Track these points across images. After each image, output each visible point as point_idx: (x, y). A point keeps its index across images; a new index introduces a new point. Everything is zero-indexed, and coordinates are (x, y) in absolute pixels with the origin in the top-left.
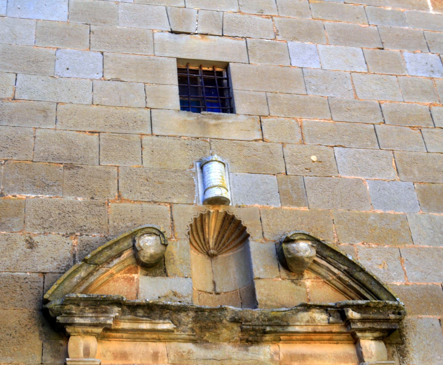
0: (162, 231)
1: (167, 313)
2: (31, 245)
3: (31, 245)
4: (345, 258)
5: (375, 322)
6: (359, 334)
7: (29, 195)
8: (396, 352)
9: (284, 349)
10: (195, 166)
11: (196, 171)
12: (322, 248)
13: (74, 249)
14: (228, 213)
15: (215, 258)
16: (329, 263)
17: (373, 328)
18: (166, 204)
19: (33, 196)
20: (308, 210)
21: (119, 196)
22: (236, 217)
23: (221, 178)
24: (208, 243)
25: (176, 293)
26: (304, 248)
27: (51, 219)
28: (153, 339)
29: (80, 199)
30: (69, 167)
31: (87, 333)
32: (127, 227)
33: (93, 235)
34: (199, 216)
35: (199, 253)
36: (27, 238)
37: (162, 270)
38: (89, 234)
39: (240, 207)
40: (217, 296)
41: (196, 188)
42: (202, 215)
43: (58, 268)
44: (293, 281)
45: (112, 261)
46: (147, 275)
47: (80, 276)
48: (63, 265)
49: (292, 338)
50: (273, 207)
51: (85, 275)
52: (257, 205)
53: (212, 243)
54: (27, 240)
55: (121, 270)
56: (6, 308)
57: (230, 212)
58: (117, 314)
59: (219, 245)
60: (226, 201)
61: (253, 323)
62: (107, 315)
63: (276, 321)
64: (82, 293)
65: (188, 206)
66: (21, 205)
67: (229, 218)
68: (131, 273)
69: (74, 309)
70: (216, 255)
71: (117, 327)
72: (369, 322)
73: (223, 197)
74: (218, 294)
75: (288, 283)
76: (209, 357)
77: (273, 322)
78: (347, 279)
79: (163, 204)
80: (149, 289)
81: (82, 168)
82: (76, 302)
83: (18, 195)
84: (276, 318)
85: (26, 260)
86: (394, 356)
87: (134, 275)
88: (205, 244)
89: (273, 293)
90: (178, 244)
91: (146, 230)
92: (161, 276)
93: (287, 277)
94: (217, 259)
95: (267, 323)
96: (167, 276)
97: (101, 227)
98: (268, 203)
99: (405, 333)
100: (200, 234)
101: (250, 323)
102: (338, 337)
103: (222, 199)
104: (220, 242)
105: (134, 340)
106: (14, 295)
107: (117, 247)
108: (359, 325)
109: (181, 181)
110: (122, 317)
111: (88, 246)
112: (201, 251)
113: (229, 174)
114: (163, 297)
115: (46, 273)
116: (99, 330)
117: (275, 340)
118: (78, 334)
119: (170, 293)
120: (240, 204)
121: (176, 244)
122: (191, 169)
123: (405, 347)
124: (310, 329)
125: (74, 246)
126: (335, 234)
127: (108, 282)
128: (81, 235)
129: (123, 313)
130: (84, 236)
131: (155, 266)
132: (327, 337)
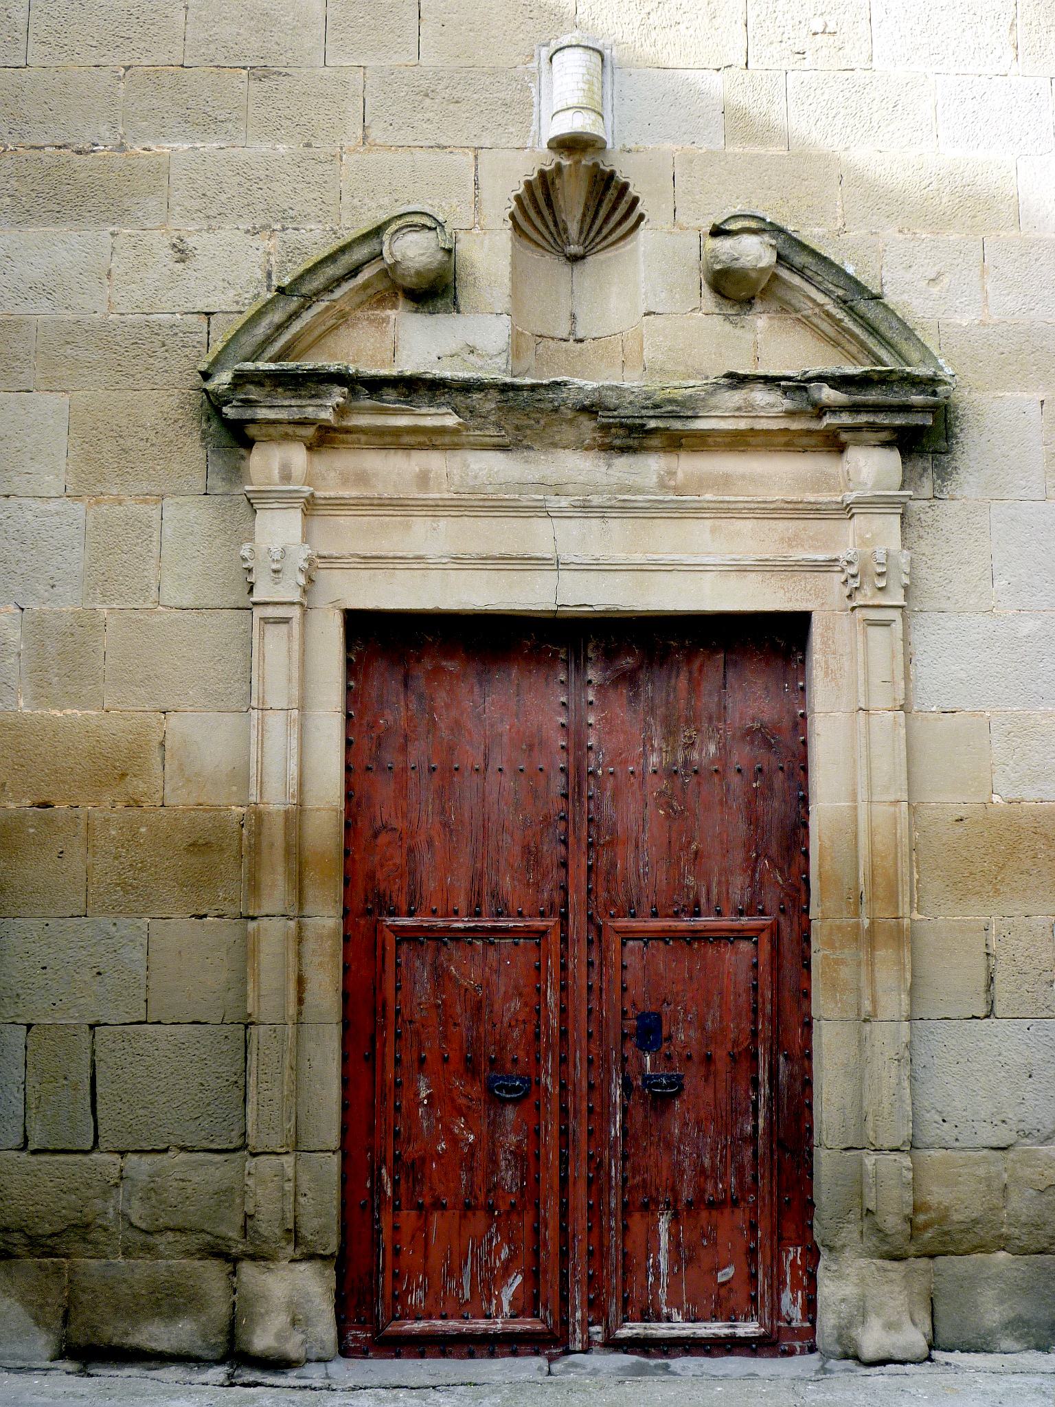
0: (440, 219)
1: (443, 394)
2: (182, 253)
3: (182, 253)
4: (840, 271)
5: (881, 412)
6: (844, 437)
7: (175, 145)
8: (930, 471)
9: (688, 465)
10: (536, 57)
12: (793, 252)
13: (268, 261)
14: (602, 167)
15: (580, 263)
16: (808, 280)
17: (873, 423)
19: (186, 146)
20: (786, 153)
21: (365, 137)
23: (586, 87)
24: (566, 230)
26: (753, 252)
27: (223, 197)
28: (419, 444)
29: (282, 148)
30: (260, 73)
31: (286, 438)
32: (380, 207)
33: (308, 227)
34: (536, 175)
36: (175, 241)
38: (300, 226)
40: (580, 345)
41: (536, 109)
42: (542, 174)
43: (237, 303)
44: (727, 317)
45: (339, 285)
46: (416, 312)
47: (271, 322)
48: (247, 296)
49: (702, 442)
50: (705, 146)
51: (282, 320)
52: (668, 146)
53: (573, 228)
54: (174, 246)
55: (362, 303)
56: (137, 387)
58: (341, 400)
59: (588, 234)
61: (622, 412)
62: (319, 402)
63: (670, 408)
64: (271, 360)
66: (160, 171)
68: (384, 308)
69: (254, 393)
70: (583, 257)
71: (344, 423)
72: (868, 412)
74: (581, 341)
76: (530, 478)
77: (663, 410)
78: (840, 315)
80: (416, 344)
81: (287, 74)
82: (258, 379)
83: (153, 147)
84: (671, 401)
85: (172, 288)
86: (924, 479)
87: (389, 312)
90: (486, 242)
91: (408, 219)
92: (445, 312)
93: (717, 311)
95: (651, 413)
96: (458, 312)
97: (325, 208)
99: (957, 430)
100: (546, 212)
101: (615, 413)
102: (805, 441)
104: (591, 227)
105: (384, 447)
106: (151, 361)
107: (346, 257)
108: (846, 419)
109: (502, 95)
110: (354, 404)
111: (297, 252)
115: (213, 313)
116: (310, 432)
117: (669, 446)
118: (271, 439)
120: (633, 146)
121: (482, 243)
123: (953, 459)
124: (742, 425)
125: (269, 253)
126: (840, 211)
127: (337, 328)
128: (284, 229)
129: (354, 393)
130: (290, 231)
131: (434, 291)
132: (783, 439)
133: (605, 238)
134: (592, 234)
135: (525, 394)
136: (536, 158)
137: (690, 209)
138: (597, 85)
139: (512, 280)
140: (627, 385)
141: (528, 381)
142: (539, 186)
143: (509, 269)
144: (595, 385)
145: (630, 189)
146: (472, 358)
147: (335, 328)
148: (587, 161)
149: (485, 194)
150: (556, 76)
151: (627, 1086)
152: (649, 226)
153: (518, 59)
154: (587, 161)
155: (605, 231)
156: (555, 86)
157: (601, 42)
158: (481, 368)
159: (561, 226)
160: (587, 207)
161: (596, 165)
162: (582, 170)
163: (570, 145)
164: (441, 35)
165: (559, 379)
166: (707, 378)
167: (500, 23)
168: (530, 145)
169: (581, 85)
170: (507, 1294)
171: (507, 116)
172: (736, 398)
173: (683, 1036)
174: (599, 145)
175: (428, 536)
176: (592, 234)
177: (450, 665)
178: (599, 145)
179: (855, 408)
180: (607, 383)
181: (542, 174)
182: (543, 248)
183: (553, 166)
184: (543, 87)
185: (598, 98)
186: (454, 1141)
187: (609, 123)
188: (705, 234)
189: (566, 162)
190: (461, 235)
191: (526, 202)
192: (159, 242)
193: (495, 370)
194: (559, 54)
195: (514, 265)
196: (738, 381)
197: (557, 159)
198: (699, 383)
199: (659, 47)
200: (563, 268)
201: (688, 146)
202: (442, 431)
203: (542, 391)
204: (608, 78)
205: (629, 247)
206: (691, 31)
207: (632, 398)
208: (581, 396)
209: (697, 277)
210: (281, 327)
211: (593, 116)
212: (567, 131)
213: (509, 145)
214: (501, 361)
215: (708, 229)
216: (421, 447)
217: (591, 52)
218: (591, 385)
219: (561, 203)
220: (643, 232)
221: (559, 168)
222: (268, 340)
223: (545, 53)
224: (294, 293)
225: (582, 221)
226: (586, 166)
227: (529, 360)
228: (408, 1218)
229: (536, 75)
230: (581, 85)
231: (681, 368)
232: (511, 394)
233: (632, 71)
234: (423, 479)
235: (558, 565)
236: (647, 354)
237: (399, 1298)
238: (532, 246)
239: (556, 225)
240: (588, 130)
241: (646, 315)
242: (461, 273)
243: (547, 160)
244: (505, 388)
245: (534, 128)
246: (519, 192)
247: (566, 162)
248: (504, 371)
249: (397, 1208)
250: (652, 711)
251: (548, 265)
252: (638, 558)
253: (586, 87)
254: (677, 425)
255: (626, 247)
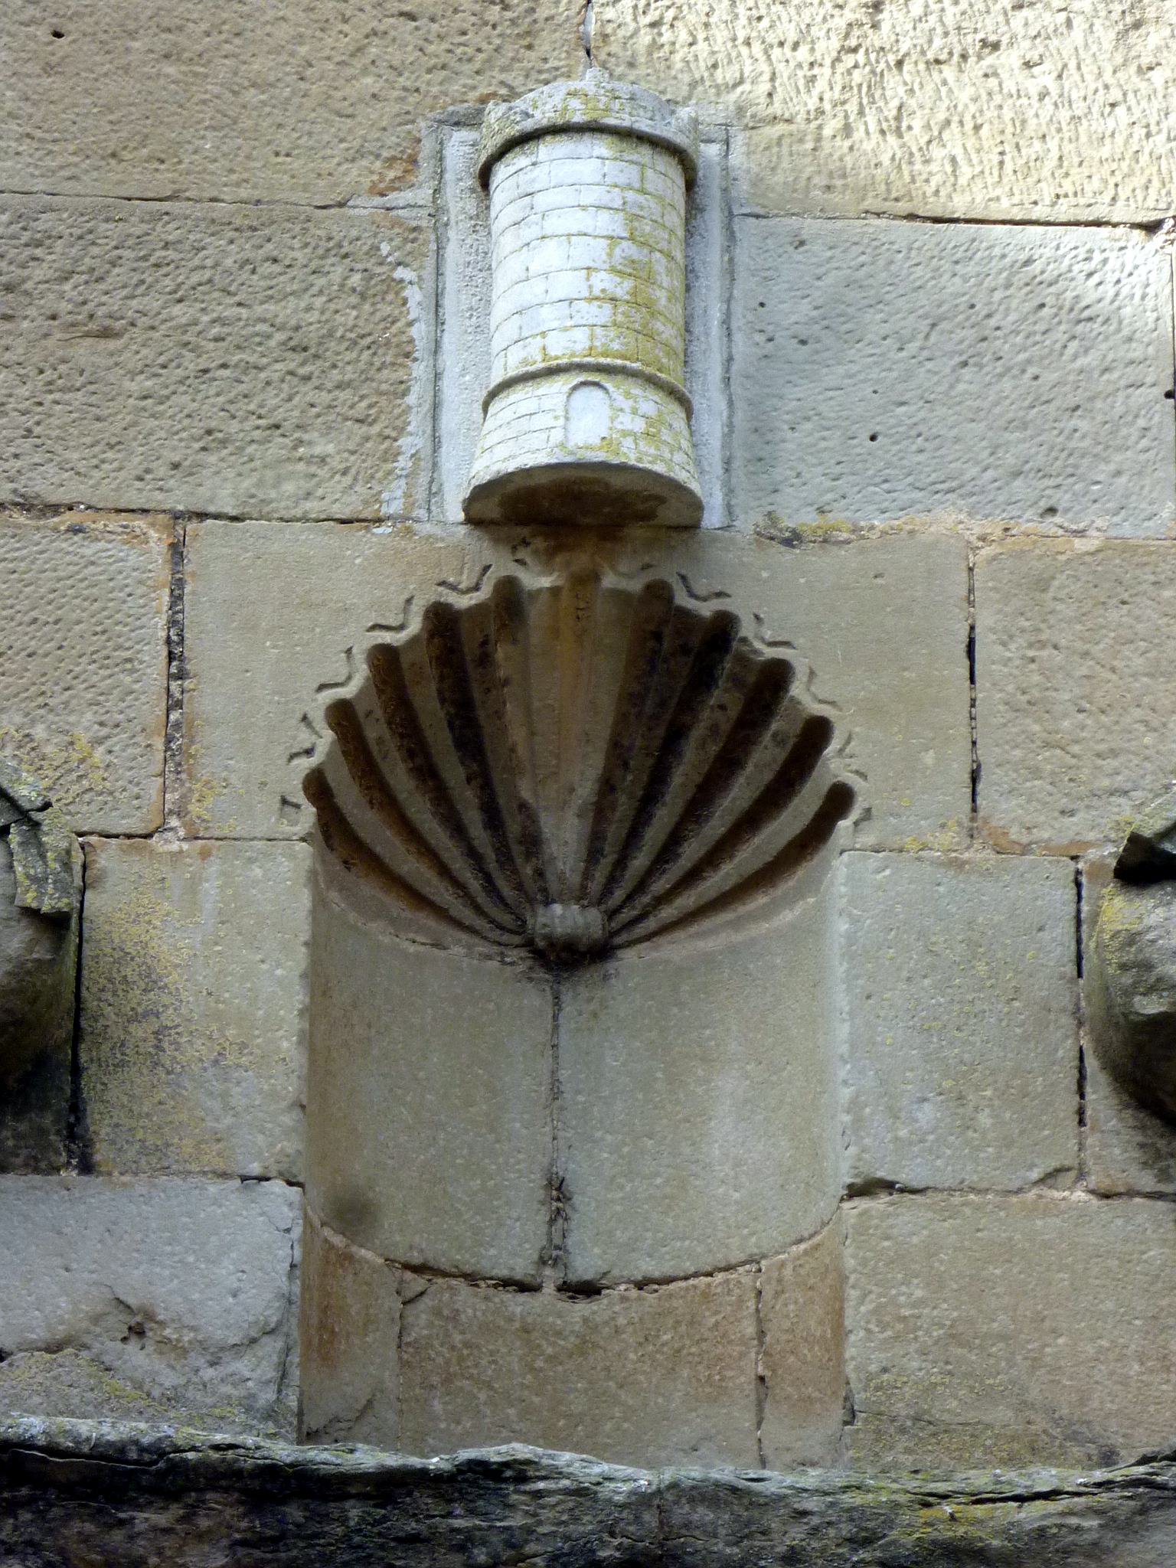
10: (426, 168)
11: (437, 212)
14: (682, 599)
18: (139, 523)
22: (747, 629)
23: (622, 288)
24: (533, 842)
25: (150, 1316)
35: (451, 934)
37: (48, 1120)
39: (793, 540)
40: (582, 1308)
41: (420, 370)
42: (441, 619)
50: (1099, 528)
52: (947, 519)
53: (564, 837)
57: (701, 587)
59: (621, 863)
60: (436, 614)
65: (335, 538)
67: (695, 641)
73: (623, 468)
74: (588, 1290)
79: (114, 523)
88: (505, 858)
89: (1002, 1322)
90: (210, 888)
92: (34, 1166)
93: (1147, 1181)
94: (606, 978)
96: (87, 1167)
98: (1062, 499)
100: (453, 771)
103: (617, 481)
104: (633, 836)
109: (286, 311)
112: (467, 915)
113: (731, 235)
114: (32, 1348)
119: (96, 1319)
120: (806, 519)
121: (193, 887)
122: (395, 198)
133: (693, 876)
134: (640, 862)
135: (354, 1512)
136: (447, 561)
137: (1036, 772)
138: (668, 280)
139: (310, 1042)
140: (777, 1480)
141: (368, 1458)
142: (431, 671)
143: (299, 997)
144: (645, 1480)
145: (797, 689)
146: (137, 1358)
148: (621, 577)
149: (208, 698)
150: (506, 243)
152: (868, 838)
153: (356, 174)
154: (621, 577)
155: (691, 851)
156: (502, 279)
157: (685, 113)
158: (173, 1399)
159: (513, 827)
160: (618, 754)
161: (658, 592)
162: (602, 611)
163: (543, 509)
164: (49, 69)
165: (494, 1453)
166: (1108, 1458)
167: (283, 32)
168: (395, 508)
169: (603, 281)
171: (307, 393)
174: (669, 514)
176: (640, 862)
178: (669, 514)
180: (692, 1472)
181: (441, 619)
182: (441, 913)
183: (484, 594)
184: (451, 281)
185: (668, 332)
187: (712, 425)
188: (1097, 868)
189: (537, 580)
190: (108, 858)
191: (375, 731)
193: (227, 1410)
194: (518, 160)
195: (319, 981)
197: (504, 566)
198: (1079, 1478)
199: (916, 137)
200: (518, 998)
201: (1029, 523)
203: (426, 1501)
204: (713, 256)
205: (787, 916)
206: (1044, 76)
207: (796, 1535)
208: (587, 1525)
209: (1064, 1042)
211: (650, 402)
212: (542, 459)
213: (312, 506)
214: (254, 1371)
215: (1109, 853)
217: (645, 154)
218: (628, 1478)
219: (517, 734)
220: (847, 866)
221: (509, 601)
223: (461, 150)
225: (600, 810)
226: (618, 595)
227: (370, 1366)
229: (424, 238)
230: (603, 281)
231: (1002, 1414)
232: (295, 1513)
233: (809, 226)
236: (860, 1352)
238: (397, 906)
239: (493, 818)
240: (630, 454)
241: (856, 1191)
242: (105, 1010)
243: (472, 572)
244: (269, 1487)
245: (412, 442)
246: (348, 692)
247: (537, 580)
248: (270, 1415)
251: (451, 981)
253: (622, 288)
255: (775, 917)
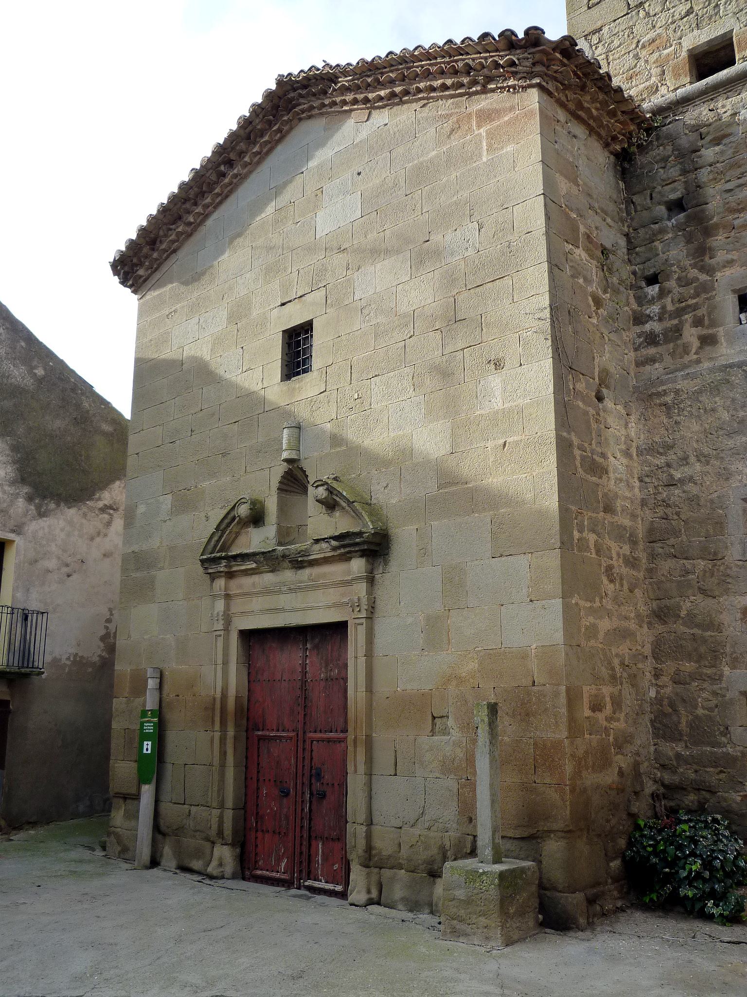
75: (326, 517)
131: (257, 518)
147: (236, 537)
151: (311, 794)
170: (283, 865)
172: (317, 547)
173: (327, 777)
175: (257, 603)
177: (274, 645)
179: (344, 546)
186: (272, 809)
192: (203, 515)
196: (317, 541)
202: (252, 569)
210: (218, 541)
216: (252, 574)
222: (215, 546)
224: (221, 528)
228: (260, 834)
234: (254, 584)
235: (283, 610)
237: (256, 862)
242: (266, 513)
249: (257, 831)
250: (322, 658)
252: (303, 606)
254: (306, 558)
